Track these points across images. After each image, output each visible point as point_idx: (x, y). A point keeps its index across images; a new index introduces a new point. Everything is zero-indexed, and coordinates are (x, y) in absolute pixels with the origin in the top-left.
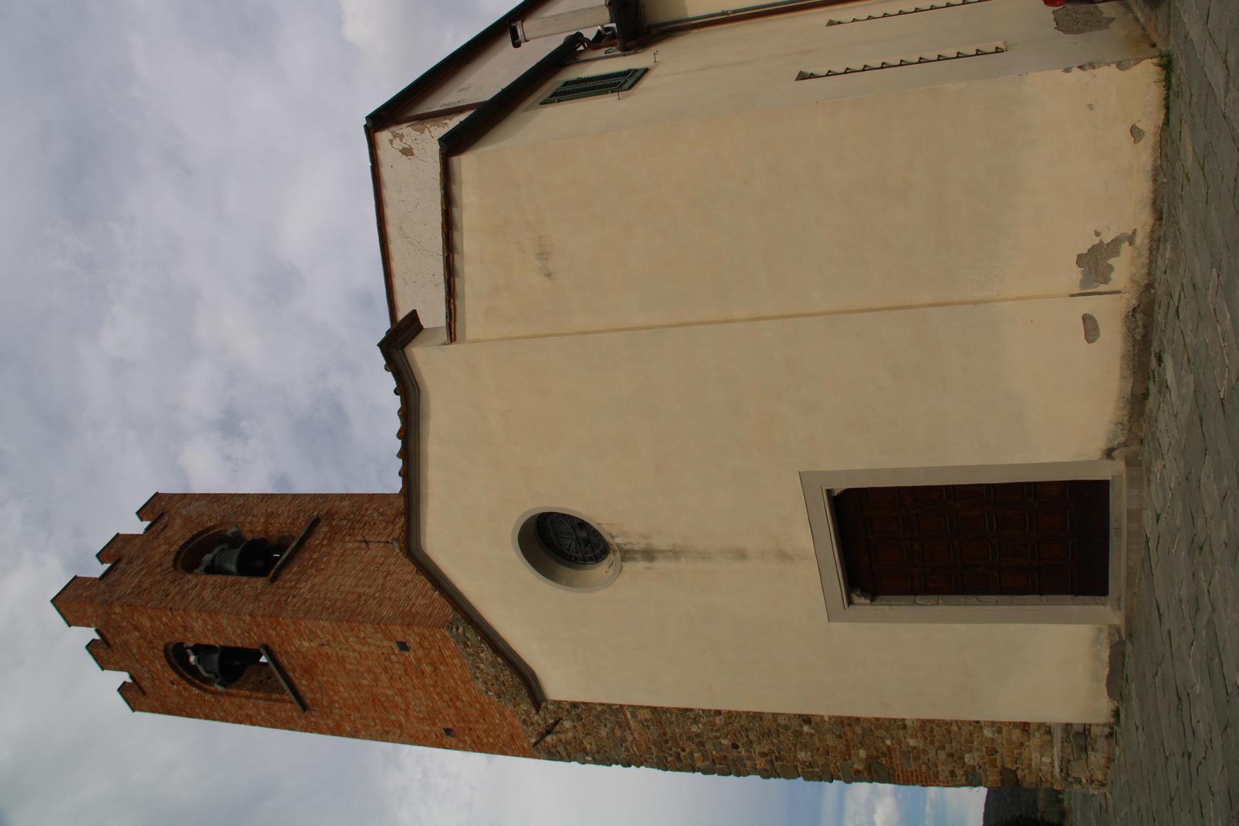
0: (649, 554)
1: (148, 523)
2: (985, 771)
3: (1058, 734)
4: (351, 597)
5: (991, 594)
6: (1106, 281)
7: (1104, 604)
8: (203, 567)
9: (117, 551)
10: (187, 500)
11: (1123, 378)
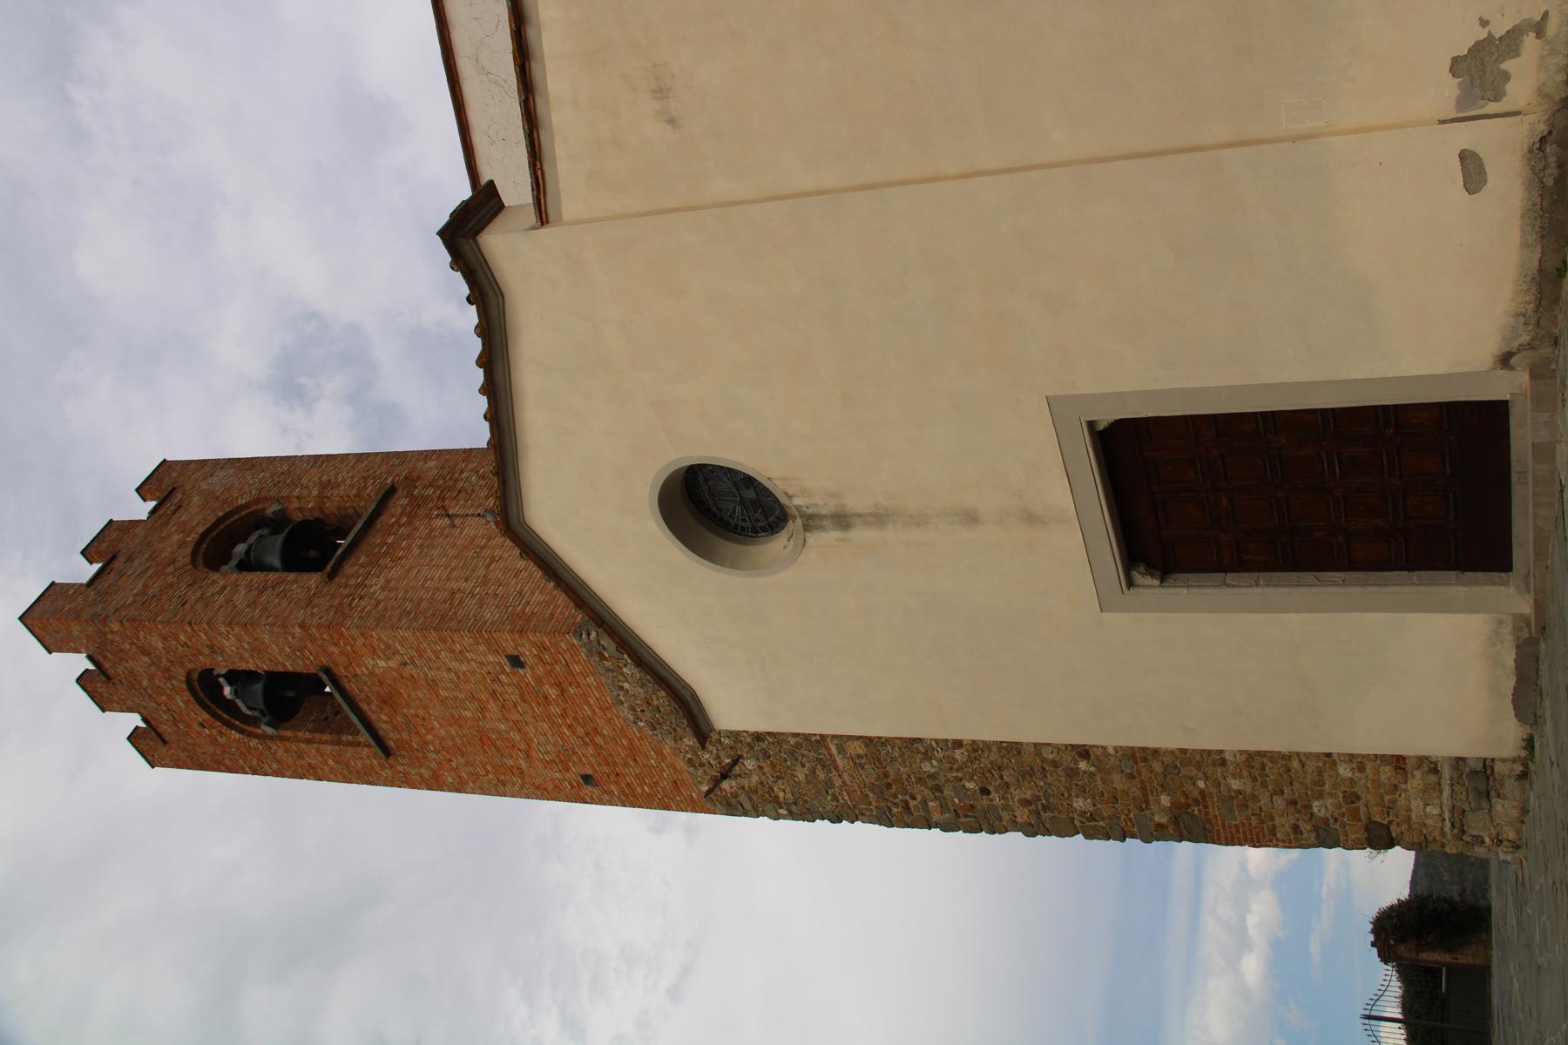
0: (842, 520)
2: (1344, 825)
3: (1446, 773)
4: (440, 596)
5: (1336, 570)
6: (1497, 98)
7: (1506, 584)
8: (234, 562)
9: (109, 546)
10: (207, 469)
11: (1525, 245)
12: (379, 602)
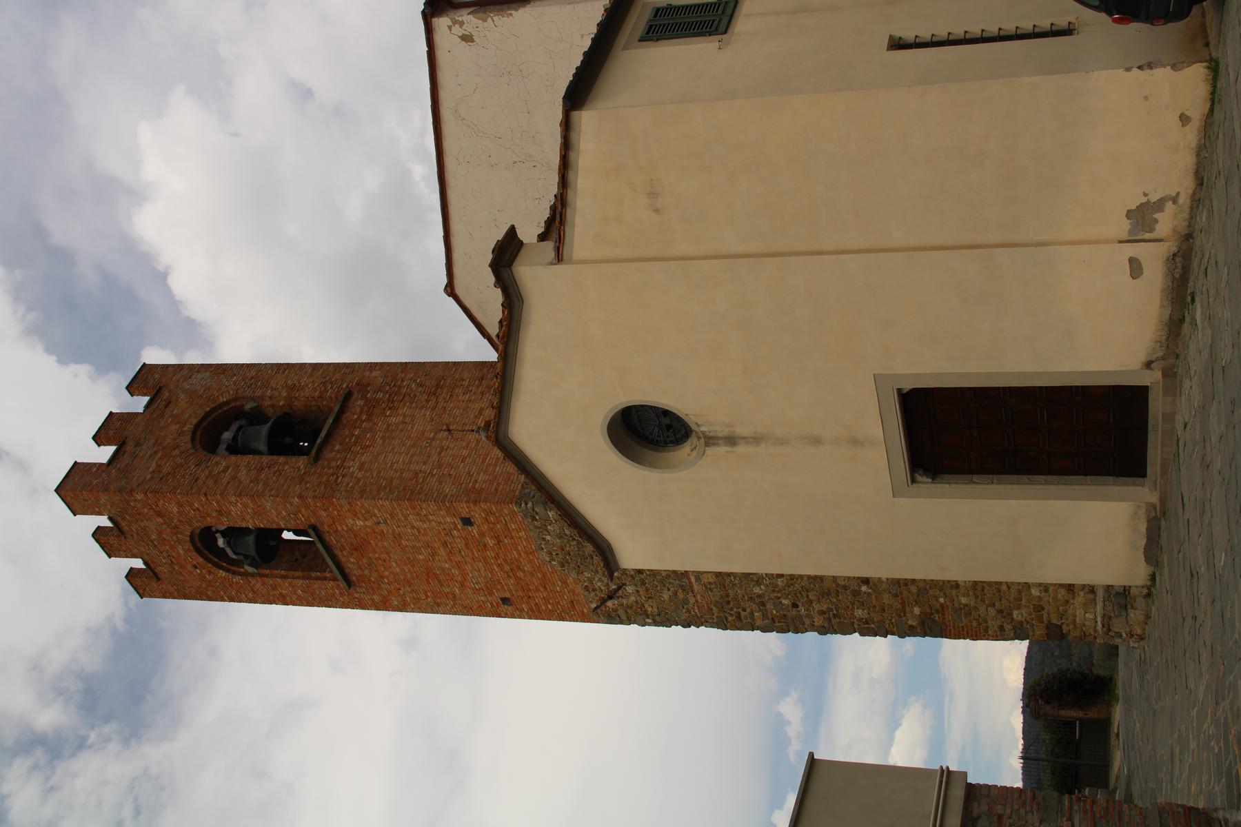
0: (731, 441)
1: (147, 399)
2: (1032, 626)
3: (1100, 594)
6: (1151, 230)
7: (1143, 485)
8: (223, 446)
11: (1162, 306)
12: (359, 480)
